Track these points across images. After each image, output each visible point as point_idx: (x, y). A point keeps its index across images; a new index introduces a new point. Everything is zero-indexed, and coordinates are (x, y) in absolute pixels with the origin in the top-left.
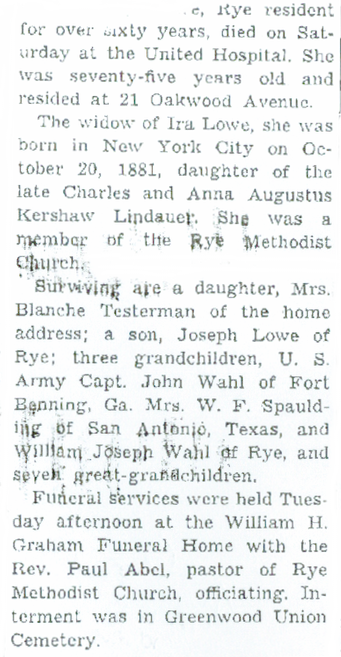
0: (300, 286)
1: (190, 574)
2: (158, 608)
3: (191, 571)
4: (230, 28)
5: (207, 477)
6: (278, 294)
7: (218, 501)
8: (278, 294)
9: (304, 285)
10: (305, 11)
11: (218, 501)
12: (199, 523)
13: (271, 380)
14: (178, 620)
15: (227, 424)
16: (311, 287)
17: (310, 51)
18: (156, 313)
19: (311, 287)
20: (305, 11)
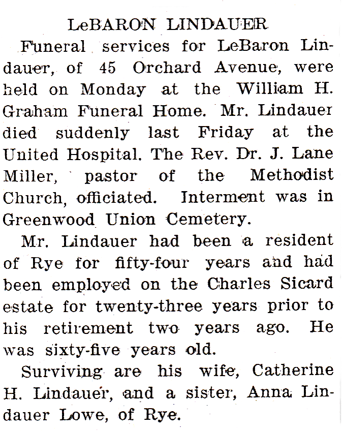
0: (228, 107)
1: (331, 259)
2: (139, 406)
3: (147, 198)
4: (312, 171)
5: (31, 178)
6: (235, 397)
7: (323, 68)
8: (235, 397)
9: (232, 106)
10: (303, 240)
11: (323, 68)
12: (286, 370)
13: (130, 412)
14: (15, 114)
15: (152, 149)
16: (239, 109)
17: (61, 131)
18: (222, 199)
19: (239, 109)
20: (303, 240)
